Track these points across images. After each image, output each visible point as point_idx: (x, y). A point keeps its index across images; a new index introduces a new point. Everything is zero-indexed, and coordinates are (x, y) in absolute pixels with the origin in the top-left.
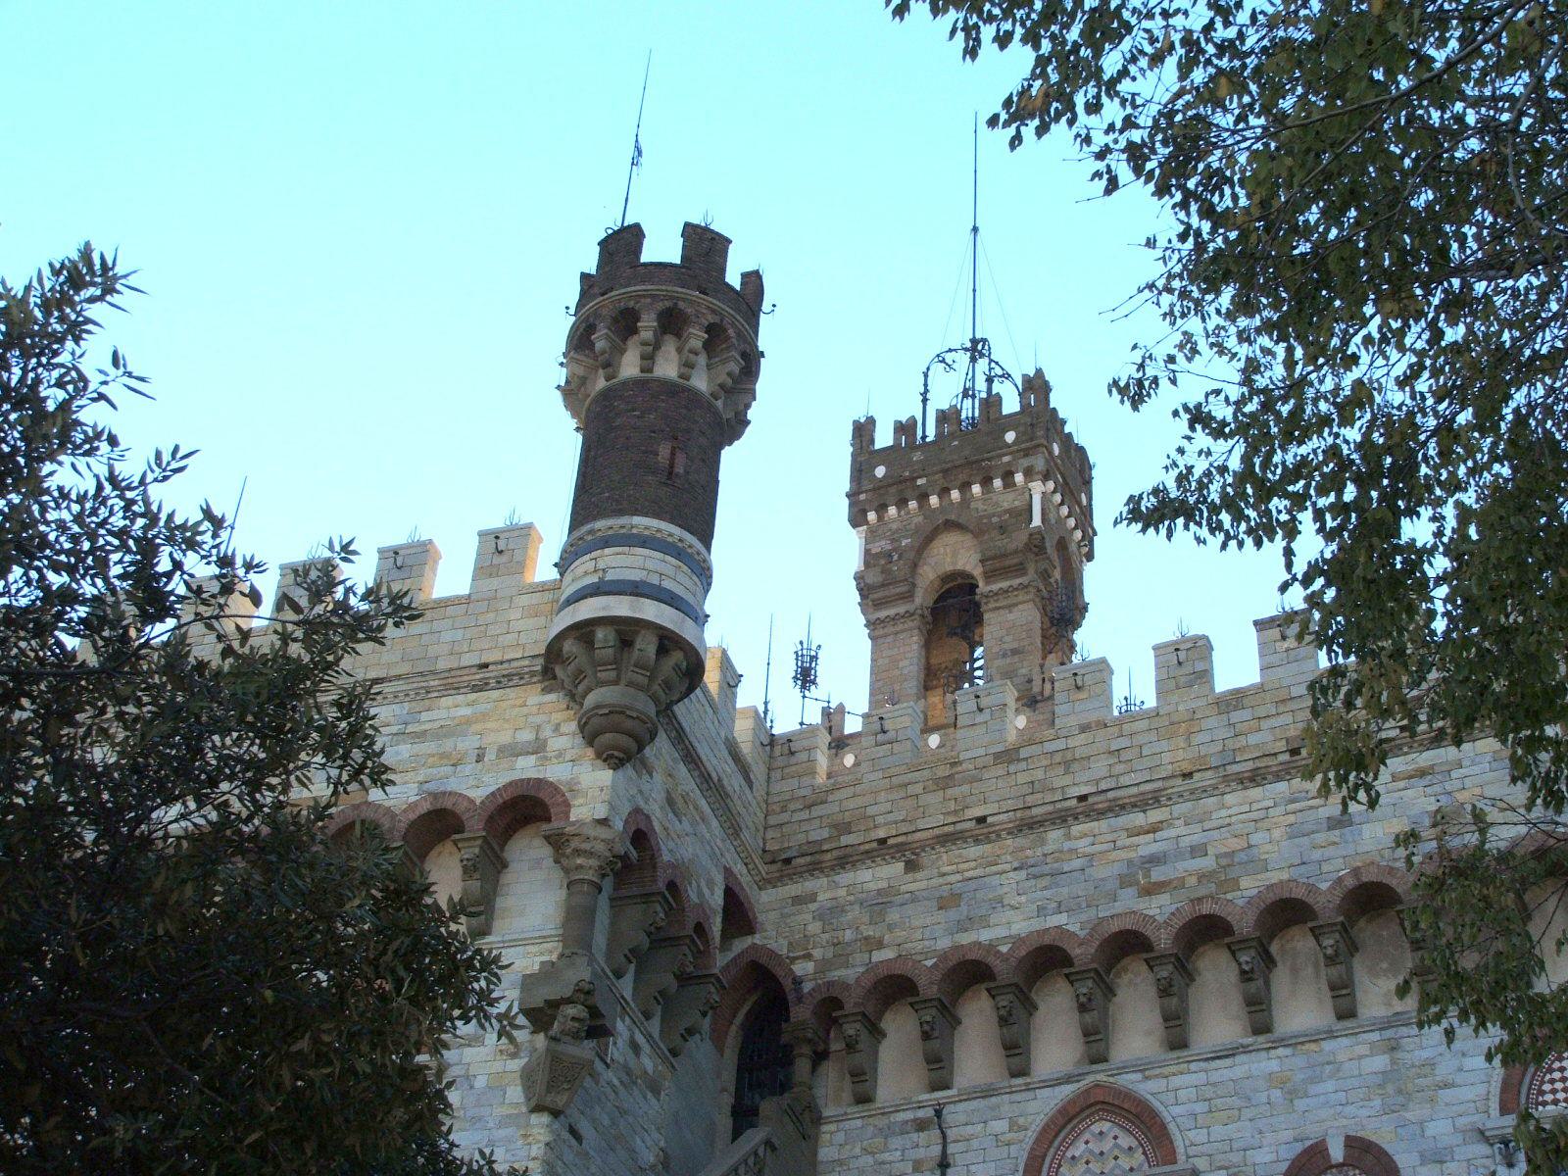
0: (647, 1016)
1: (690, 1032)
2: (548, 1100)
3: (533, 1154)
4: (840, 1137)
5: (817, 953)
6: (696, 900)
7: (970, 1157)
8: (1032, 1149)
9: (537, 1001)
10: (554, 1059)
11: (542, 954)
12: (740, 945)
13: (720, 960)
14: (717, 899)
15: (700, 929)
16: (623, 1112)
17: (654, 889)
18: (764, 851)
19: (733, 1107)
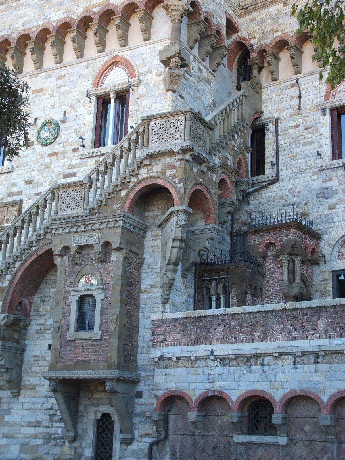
0: (203, 60)
1: (219, 64)
2: (171, 88)
3: (168, 104)
4: (268, 92)
5: (257, 36)
6: (216, 23)
7: (307, 94)
8: (327, 89)
9: (164, 58)
10: (171, 75)
11: (166, 44)
12: (234, 37)
13: (227, 42)
14: (224, 22)
15: (218, 32)
16: (198, 90)
17: (200, 20)
18: (240, 6)
19: (237, 87)
